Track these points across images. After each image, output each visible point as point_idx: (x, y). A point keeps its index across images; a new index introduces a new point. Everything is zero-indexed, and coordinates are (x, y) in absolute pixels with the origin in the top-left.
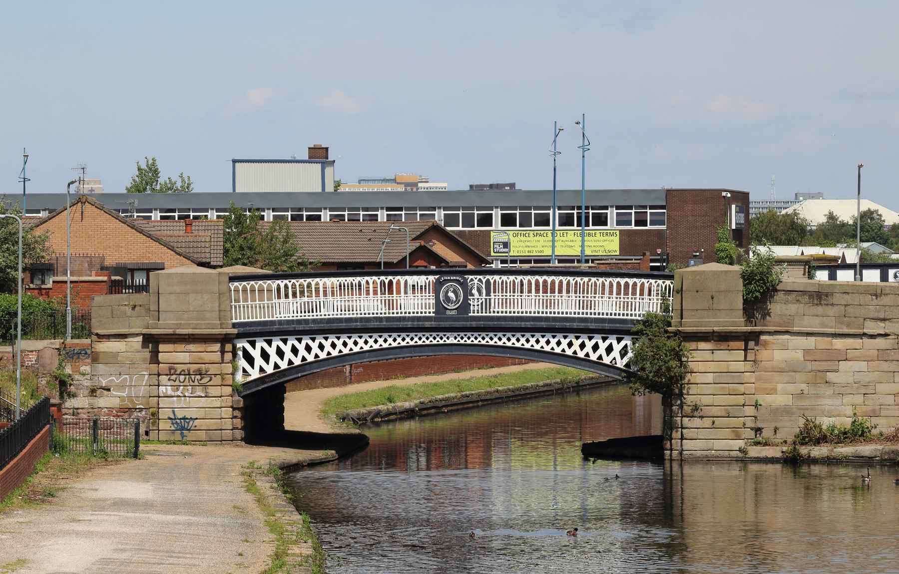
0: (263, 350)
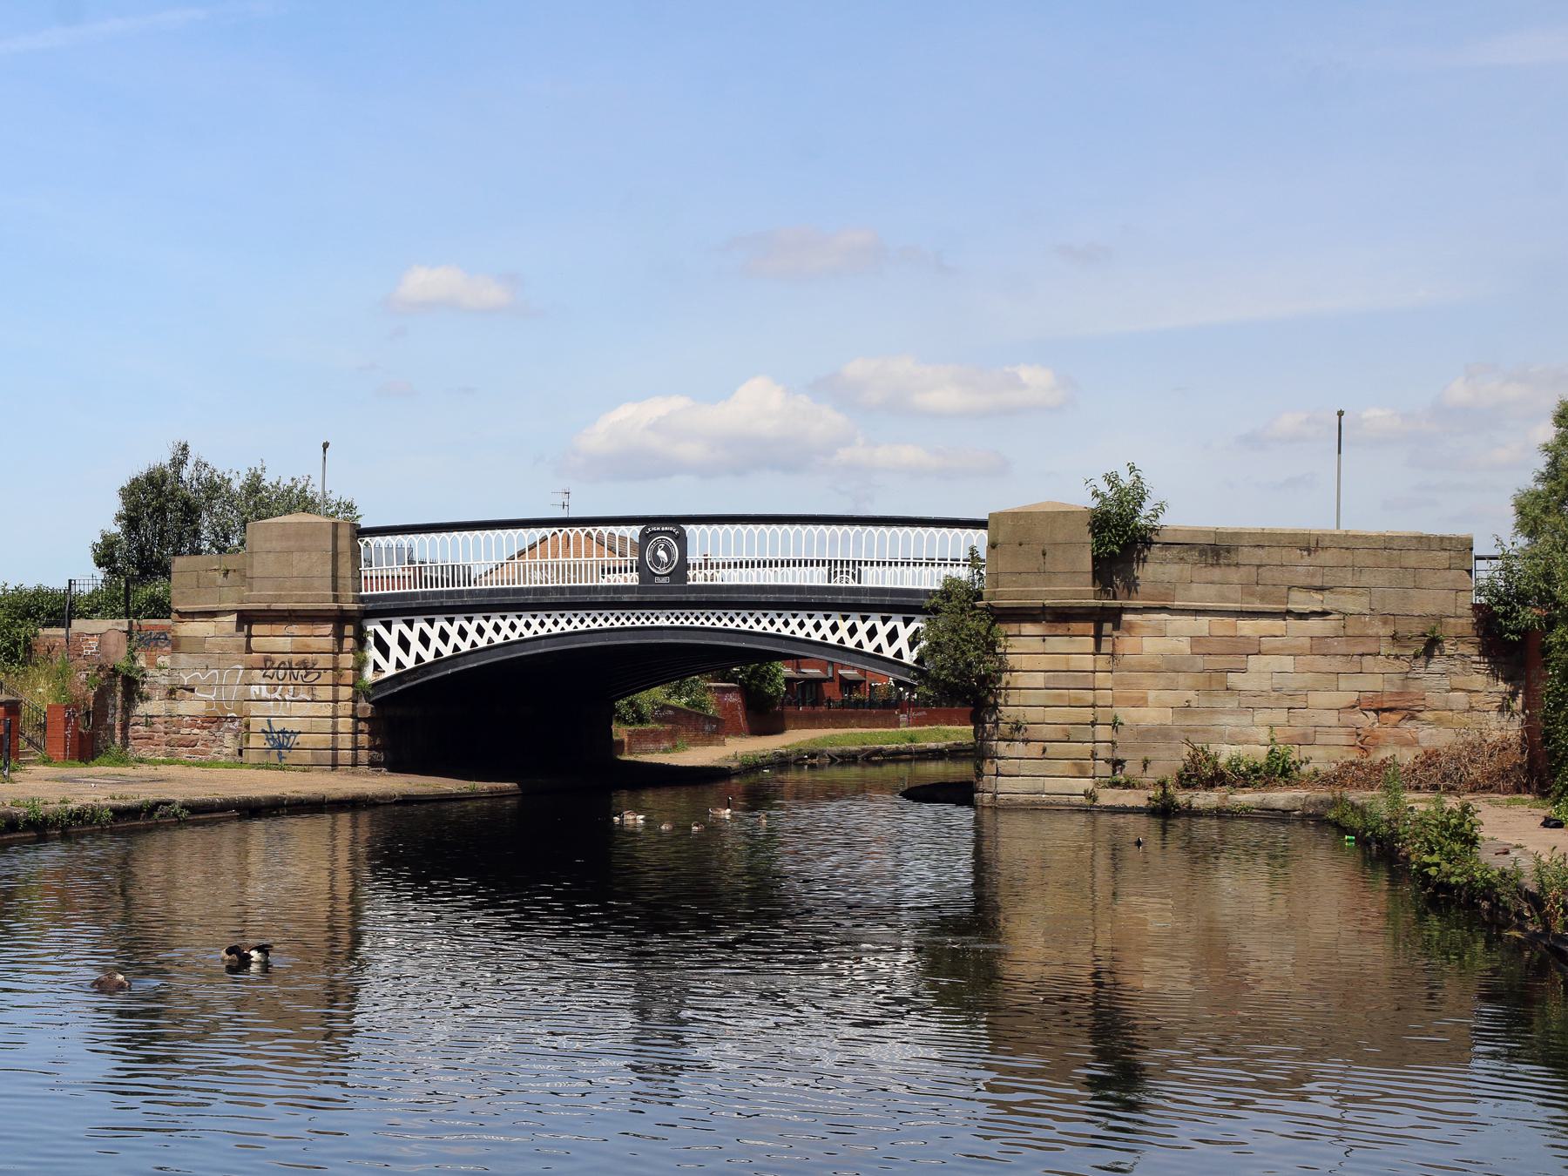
0: (401, 635)
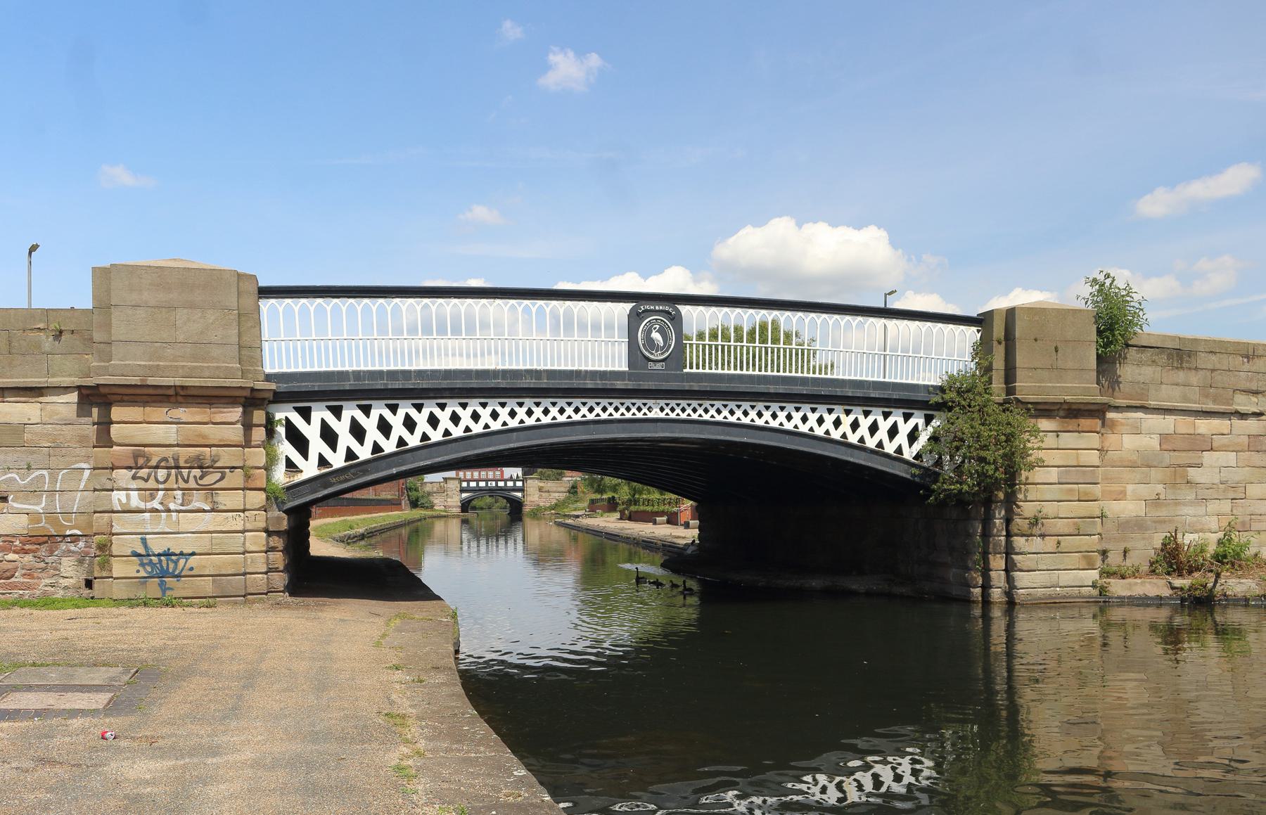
0: (324, 425)
